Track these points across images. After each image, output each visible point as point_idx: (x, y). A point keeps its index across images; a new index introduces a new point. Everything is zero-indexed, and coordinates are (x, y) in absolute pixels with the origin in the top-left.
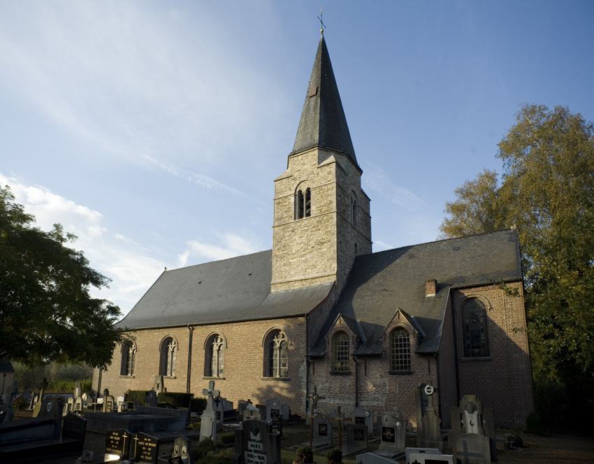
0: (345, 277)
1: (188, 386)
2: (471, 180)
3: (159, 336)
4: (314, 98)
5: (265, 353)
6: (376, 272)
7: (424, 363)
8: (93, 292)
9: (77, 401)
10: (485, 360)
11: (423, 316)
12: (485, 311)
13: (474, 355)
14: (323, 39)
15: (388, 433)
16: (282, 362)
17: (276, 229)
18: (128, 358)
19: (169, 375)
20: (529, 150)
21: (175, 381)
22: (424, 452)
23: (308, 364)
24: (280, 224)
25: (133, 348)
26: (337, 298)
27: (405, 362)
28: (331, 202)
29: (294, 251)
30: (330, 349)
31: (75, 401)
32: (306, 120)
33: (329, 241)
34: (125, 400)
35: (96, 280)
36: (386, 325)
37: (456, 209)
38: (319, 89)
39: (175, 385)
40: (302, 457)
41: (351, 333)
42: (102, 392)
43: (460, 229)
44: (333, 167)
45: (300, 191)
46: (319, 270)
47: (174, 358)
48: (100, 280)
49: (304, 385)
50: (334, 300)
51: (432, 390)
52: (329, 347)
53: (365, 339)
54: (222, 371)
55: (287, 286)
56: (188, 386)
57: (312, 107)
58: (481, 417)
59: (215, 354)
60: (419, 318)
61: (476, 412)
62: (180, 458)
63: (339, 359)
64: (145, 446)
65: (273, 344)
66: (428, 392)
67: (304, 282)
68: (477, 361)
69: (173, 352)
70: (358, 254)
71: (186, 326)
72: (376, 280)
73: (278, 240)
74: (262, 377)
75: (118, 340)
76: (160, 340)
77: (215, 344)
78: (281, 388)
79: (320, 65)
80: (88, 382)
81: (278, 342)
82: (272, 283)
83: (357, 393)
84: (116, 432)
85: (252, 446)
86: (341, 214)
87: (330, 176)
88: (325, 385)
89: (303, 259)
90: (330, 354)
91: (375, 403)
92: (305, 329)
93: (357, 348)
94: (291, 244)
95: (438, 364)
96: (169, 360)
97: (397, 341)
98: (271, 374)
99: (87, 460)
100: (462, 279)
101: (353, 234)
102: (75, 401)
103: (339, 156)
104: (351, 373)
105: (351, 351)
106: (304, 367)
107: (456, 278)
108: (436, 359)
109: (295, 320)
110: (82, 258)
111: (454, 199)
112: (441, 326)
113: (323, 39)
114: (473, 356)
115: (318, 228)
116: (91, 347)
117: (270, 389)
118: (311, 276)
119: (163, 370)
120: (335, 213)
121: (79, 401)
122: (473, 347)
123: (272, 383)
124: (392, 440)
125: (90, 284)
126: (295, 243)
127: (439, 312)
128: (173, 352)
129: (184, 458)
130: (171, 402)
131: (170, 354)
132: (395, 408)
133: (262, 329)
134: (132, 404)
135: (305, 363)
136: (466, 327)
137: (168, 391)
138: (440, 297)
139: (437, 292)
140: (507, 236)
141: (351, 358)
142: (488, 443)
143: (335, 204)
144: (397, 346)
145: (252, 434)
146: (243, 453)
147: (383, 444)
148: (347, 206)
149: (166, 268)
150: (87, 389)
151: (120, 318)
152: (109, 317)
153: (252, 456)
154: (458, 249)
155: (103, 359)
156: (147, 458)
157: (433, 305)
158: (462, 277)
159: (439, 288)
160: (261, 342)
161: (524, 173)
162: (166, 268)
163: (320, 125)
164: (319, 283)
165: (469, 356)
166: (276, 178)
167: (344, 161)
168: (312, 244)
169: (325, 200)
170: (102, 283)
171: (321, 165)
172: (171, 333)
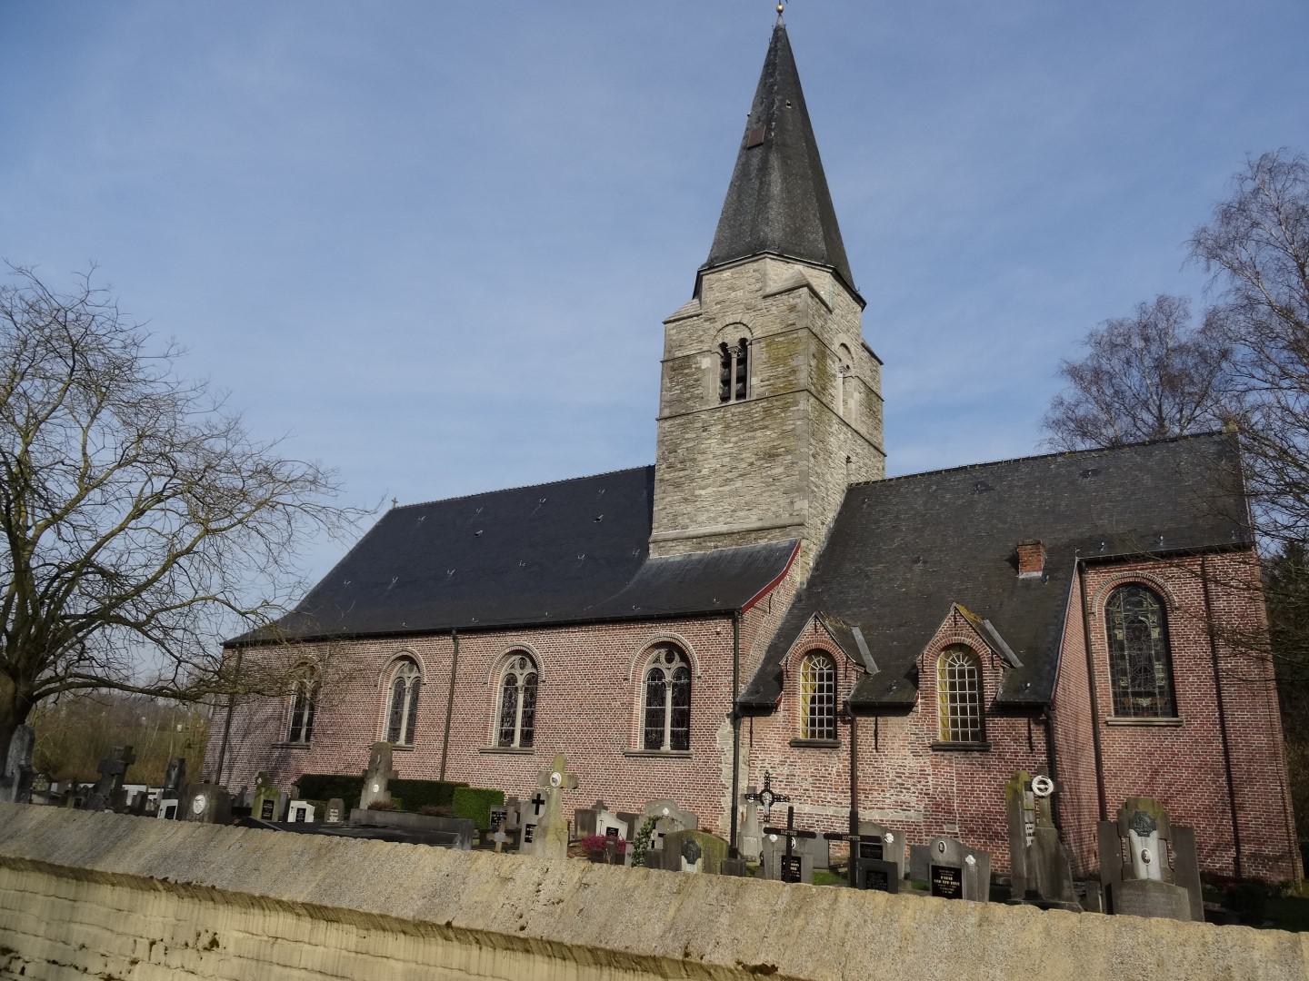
13: (1139, 711)
15: (947, 879)
17: (667, 424)
24: (677, 412)
26: (808, 575)
29: (705, 472)
50: (798, 579)
51: (1035, 786)
61: (1155, 834)
73: (668, 447)
82: (651, 539)
83: (853, 789)
94: (699, 457)
107: (1090, 538)
108: (735, 622)
114: (1136, 715)
122: (1136, 694)
149: (395, 502)
162: (395, 502)
164: (762, 542)
165: (1127, 714)
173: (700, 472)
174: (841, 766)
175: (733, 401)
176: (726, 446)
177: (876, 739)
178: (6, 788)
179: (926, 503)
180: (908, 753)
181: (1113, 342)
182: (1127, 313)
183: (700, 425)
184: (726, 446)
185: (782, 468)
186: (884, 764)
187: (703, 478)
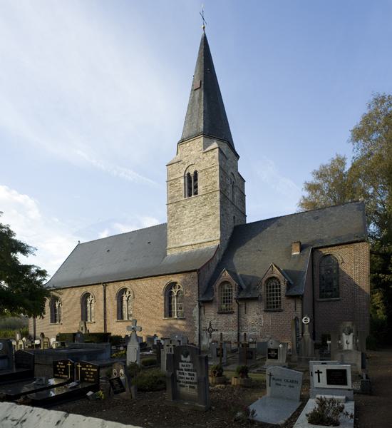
0: (226, 242)
1: (105, 328)
2: (325, 164)
3: (78, 293)
4: (198, 91)
5: (165, 300)
6: (251, 238)
7: (292, 303)
8: (22, 259)
9: (19, 343)
10: (335, 301)
11: (291, 269)
12: (338, 265)
15: (273, 353)
16: (179, 306)
18: (55, 311)
19: (89, 321)
20: (375, 136)
21: (94, 326)
22: (325, 363)
23: (200, 307)
24: (172, 202)
25: (91, 299)
27: (277, 303)
29: (185, 223)
30: (217, 295)
31: (17, 343)
33: (214, 214)
34: (57, 340)
35: (23, 249)
36: (261, 276)
37: (312, 188)
38: (203, 83)
39: (95, 327)
40: (215, 372)
41: (234, 283)
42: (38, 335)
43: (314, 204)
45: (189, 174)
47: (92, 308)
48: (27, 249)
49: (197, 323)
52: (216, 294)
53: (244, 287)
54: (131, 315)
56: (105, 328)
57: (197, 99)
58: (355, 338)
59: (125, 303)
60: (289, 271)
61: (352, 334)
62: (119, 378)
63: (224, 302)
64: (87, 371)
65: (171, 293)
68: (330, 301)
69: (91, 303)
70: (236, 224)
71: (100, 284)
72: (251, 244)
73: (171, 215)
75: (48, 296)
77: (124, 295)
78: (179, 325)
79: (203, 61)
80: (25, 330)
81: (175, 291)
82: (168, 247)
84: (61, 362)
85: (182, 365)
86: (223, 192)
90: (217, 298)
91: (253, 333)
92: (197, 281)
93: (239, 294)
95: (302, 304)
96: (89, 309)
97: (270, 287)
98: (170, 316)
99: (41, 383)
100: (321, 241)
102: (17, 343)
103: (221, 143)
105: (234, 296)
106: (196, 309)
109: (189, 275)
110: (10, 232)
111: (311, 179)
112: (305, 277)
113: (205, 34)
116: (27, 301)
117: (171, 327)
118: (190, 243)
119: (84, 317)
120: (219, 192)
121: (21, 343)
123: (172, 322)
124: (276, 357)
125: (19, 253)
127: (304, 266)
128: (91, 303)
129: (122, 378)
130: (93, 340)
131: (88, 305)
132: (268, 336)
133: (162, 283)
134: (64, 343)
135: (197, 306)
136: (322, 278)
137: (90, 332)
138: (303, 255)
139: (301, 250)
140: (357, 207)
141: (234, 301)
142: (360, 356)
143: (218, 184)
144: (270, 291)
145: (182, 357)
146: (175, 372)
147: (268, 361)
148: (228, 186)
150: (25, 334)
151: (48, 279)
152: (38, 278)
153: (190, 374)
154: (317, 218)
155: (38, 311)
156: (90, 380)
157: (297, 260)
159: (302, 248)
160: (161, 291)
161: (371, 154)
163: (204, 115)
165: (322, 298)
166: (168, 162)
167: (225, 147)
169: (210, 181)
170: (29, 251)
171: (207, 150)
172: (89, 289)
175: (193, 196)
178: (60, 334)
181: (321, 175)
182: (327, 161)
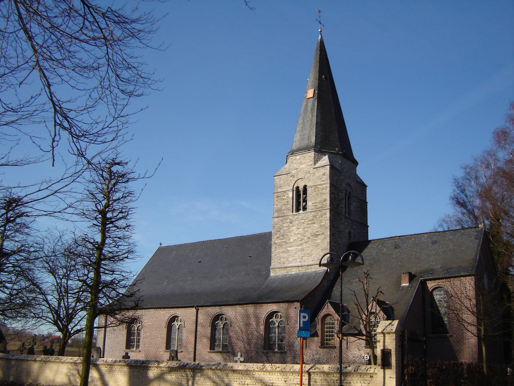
3: (165, 314)
14: (322, 39)
28: (325, 200)
29: (291, 240)
32: (304, 121)
33: (323, 234)
44: (327, 170)
45: (298, 188)
46: (314, 258)
50: (326, 285)
55: (285, 271)
57: (309, 110)
66: (366, 358)
67: (300, 269)
71: (193, 307)
74: (209, 350)
76: (167, 318)
87: (325, 176)
88: (315, 356)
89: (300, 247)
94: (289, 234)
100: (431, 271)
101: (346, 224)
104: (336, 347)
115: (313, 222)
118: (307, 263)
120: (329, 210)
126: (293, 234)
141: (336, 335)
158: (432, 269)
164: (313, 270)
168: (308, 234)
171: (316, 166)
172: (178, 312)
173: (289, 240)
174: (335, 355)
176: (299, 230)
177: (347, 345)
179: (377, 252)
180: (357, 349)
183: (289, 221)
184: (299, 230)
185: (321, 240)
186: (349, 354)
187: (291, 243)
